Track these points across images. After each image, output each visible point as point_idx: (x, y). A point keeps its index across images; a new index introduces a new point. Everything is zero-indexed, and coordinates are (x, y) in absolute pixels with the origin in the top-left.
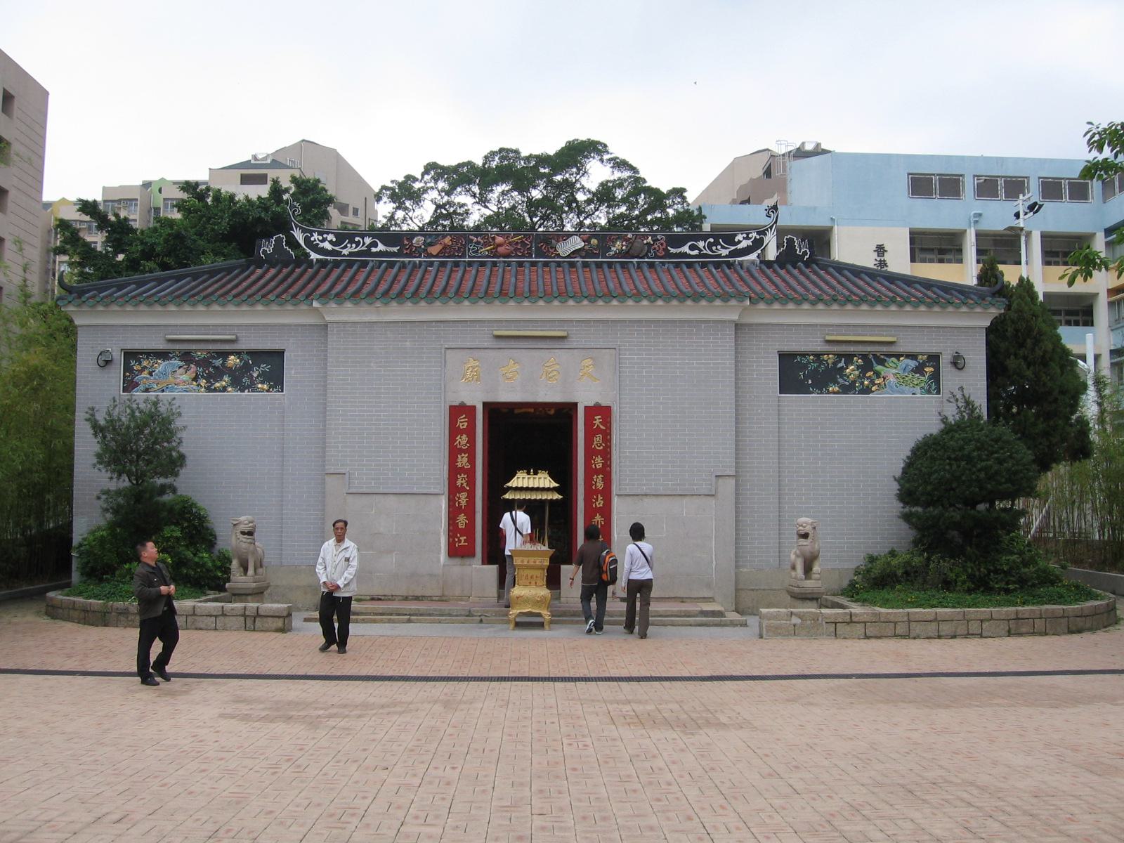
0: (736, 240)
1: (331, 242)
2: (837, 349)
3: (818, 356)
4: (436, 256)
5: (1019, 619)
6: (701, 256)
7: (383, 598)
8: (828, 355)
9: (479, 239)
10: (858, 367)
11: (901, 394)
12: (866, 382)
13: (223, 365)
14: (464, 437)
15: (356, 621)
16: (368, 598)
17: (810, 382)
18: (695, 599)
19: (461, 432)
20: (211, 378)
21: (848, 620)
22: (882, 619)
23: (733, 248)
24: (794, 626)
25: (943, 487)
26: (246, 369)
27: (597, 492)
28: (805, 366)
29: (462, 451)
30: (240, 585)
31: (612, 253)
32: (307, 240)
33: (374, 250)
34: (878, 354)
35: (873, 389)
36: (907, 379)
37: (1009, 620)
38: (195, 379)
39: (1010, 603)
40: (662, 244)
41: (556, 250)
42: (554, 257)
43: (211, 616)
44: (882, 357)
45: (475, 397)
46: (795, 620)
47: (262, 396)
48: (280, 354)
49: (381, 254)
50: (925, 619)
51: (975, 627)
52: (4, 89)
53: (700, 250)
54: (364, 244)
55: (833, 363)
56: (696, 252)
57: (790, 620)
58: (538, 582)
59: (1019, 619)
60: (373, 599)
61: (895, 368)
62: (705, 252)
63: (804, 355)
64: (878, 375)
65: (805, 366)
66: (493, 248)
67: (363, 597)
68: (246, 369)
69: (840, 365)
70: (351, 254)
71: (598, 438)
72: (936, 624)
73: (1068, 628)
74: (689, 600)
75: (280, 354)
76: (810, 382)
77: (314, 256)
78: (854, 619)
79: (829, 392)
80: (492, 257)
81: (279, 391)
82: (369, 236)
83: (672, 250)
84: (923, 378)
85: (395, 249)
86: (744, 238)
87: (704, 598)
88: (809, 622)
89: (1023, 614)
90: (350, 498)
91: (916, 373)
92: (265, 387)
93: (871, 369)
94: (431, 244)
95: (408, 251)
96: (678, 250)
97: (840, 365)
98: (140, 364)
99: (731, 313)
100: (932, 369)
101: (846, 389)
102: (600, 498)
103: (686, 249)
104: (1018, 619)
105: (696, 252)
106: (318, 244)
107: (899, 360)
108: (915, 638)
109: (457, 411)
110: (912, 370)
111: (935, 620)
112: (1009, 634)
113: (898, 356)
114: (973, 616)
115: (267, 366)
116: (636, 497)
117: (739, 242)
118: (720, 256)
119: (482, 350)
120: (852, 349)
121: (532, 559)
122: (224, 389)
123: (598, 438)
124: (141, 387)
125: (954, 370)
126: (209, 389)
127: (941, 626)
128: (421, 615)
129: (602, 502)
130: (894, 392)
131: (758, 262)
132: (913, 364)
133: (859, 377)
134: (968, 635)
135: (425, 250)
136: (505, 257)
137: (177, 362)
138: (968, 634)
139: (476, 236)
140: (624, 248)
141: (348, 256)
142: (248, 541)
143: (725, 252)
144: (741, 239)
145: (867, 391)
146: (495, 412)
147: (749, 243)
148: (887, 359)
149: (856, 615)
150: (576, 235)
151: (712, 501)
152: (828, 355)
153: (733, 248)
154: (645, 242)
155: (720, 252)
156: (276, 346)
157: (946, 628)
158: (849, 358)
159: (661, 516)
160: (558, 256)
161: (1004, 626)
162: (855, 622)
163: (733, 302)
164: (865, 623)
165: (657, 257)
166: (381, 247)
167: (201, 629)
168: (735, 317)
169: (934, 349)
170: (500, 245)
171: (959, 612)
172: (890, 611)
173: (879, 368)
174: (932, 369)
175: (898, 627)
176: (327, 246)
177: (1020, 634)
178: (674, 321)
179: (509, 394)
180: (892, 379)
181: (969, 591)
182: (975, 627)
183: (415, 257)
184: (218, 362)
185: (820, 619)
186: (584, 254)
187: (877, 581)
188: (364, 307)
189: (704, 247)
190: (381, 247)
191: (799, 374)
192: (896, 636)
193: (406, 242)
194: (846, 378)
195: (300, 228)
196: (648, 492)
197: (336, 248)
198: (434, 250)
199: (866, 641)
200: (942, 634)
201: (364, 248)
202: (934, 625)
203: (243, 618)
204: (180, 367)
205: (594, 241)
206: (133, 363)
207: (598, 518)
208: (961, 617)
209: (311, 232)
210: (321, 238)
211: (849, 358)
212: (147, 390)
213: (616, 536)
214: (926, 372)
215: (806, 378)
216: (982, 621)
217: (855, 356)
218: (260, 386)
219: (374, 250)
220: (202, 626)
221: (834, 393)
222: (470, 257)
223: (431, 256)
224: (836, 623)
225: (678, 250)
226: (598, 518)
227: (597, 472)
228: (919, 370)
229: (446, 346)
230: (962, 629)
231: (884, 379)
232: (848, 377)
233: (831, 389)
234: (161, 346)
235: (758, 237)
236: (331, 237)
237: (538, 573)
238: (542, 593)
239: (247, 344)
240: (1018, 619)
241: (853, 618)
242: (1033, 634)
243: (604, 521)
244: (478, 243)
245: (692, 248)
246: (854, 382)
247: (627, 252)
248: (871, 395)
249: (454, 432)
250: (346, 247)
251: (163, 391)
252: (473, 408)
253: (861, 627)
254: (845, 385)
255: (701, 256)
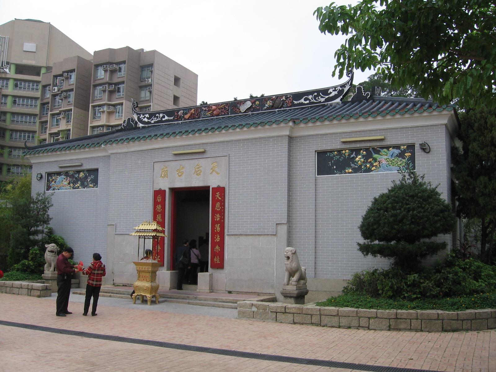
0: (329, 92)
1: (147, 118)
2: (348, 146)
3: (339, 151)
4: (188, 119)
5: (398, 319)
6: (311, 103)
7: (127, 285)
8: (345, 150)
9: (206, 109)
10: (363, 156)
11: (390, 171)
12: (368, 165)
13: (78, 176)
14: (160, 206)
15: (103, 296)
16: (122, 285)
17: (335, 167)
18: (265, 293)
19: (158, 203)
20: (75, 183)
21: (284, 311)
22: (304, 312)
23: (327, 97)
24: (253, 312)
25: (371, 228)
26: (86, 177)
27: (217, 233)
28: (332, 158)
29: (158, 213)
30: (46, 275)
31: (265, 108)
32: (139, 118)
33: (163, 119)
34: (375, 147)
35: (373, 169)
36: (393, 161)
37: (390, 319)
38: (69, 184)
39: (390, 307)
40: (290, 100)
41: (239, 110)
42: (239, 113)
43: (18, 288)
44: (378, 149)
45: (165, 185)
46: (254, 309)
47: (89, 191)
48: (97, 170)
49: (166, 121)
50: (331, 314)
51: (363, 322)
52: (175, 76)
53: (310, 100)
54: (160, 117)
55: (349, 155)
56: (308, 102)
57: (251, 309)
58: (147, 279)
59: (398, 319)
60: (123, 286)
61: (386, 155)
62: (312, 101)
63: (331, 151)
64: (375, 160)
65: (332, 158)
66: (212, 112)
67: (120, 284)
68: (86, 177)
69: (352, 156)
70: (155, 122)
71: (218, 204)
72: (338, 317)
73: (443, 328)
74: (262, 294)
75: (97, 170)
76: (335, 167)
77: (141, 125)
78: (287, 311)
79: (346, 173)
80: (212, 117)
81: (97, 187)
82: (162, 113)
83: (295, 102)
84: (404, 160)
85: (172, 118)
86: (333, 91)
87: (270, 293)
88: (261, 311)
89: (401, 315)
90: (116, 236)
91: (399, 157)
92: (92, 186)
93: (371, 156)
94: (186, 114)
95: (177, 118)
96: (299, 102)
97: (352, 156)
98: (52, 178)
99: (284, 130)
100: (410, 154)
101: (357, 170)
102: (218, 236)
103: (302, 101)
104: (397, 318)
105: (308, 102)
106: (142, 120)
107: (388, 150)
108: (324, 326)
109: (159, 194)
110: (397, 156)
111: (338, 315)
112: (390, 329)
113: (388, 148)
114: (363, 315)
115: (90, 177)
116: (236, 236)
117: (331, 93)
118: (320, 102)
119: (169, 162)
120: (358, 145)
121: (144, 267)
122: (78, 188)
123: (218, 204)
124: (52, 189)
125: (423, 153)
126: (74, 188)
127: (340, 320)
128: (121, 294)
129: (219, 239)
130: (385, 170)
131: (341, 103)
132: (397, 152)
133: (364, 162)
134: (359, 327)
135: (183, 117)
136: (217, 116)
137: (63, 177)
138: (359, 326)
139: (205, 107)
140: (271, 104)
141: (154, 123)
142: (52, 255)
143: (323, 100)
144: (332, 91)
145: (369, 170)
146: (175, 192)
147: (336, 93)
148: (381, 150)
149: (288, 308)
150: (249, 101)
151: (275, 238)
152: (345, 150)
153: (327, 97)
154: (282, 99)
155: (320, 100)
156: (96, 167)
157: (344, 321)
158: (357, 151)
159: (250, 247)
160: (240, 112)
161: (386, 323)
162: (287, 313)
163: (282, 125)
164: (294, 313)
165: (287, 107)
166: (166, 118)
167: (14, 294)
168: (287, 133)
169: (410, 141)
170: (214, 110)
171: (353, 311)
172: (365, 310)
173: (375, 156)
174: (410, 154)
175: (314, 318)
176: (146, 120)
177: (399, 330)
178: (255, 139)
179: (180, 184)
180: (384, 162)
181: (390, 297)
182: (363, 322)
183: (180, 121)
184: (77, 176)
185: (268, 309)
186: (252, 110)
187: (365, 291)
188: (120, 145)
189: (312, 98)
190: (166, 118)
191: (328, 163)
192: (312, 324)
193: (176, 114)
194: (356, 163)
195: (136, 113)
196: (242, 233)
197: (149, 121)
198: (187, 116)
199: (294, 325)
200: (341, 325)
201: (160, 119)
202: (336, 319)
203: (27, 290)
204: (64, 179)
205: (257, 103)
206: (50, 178)
207: (217, 247)
208: (355, 314)
209: (140, 114)
210: (143, 116)
211: (357, 151)
212: (54, 190)
213: (226, 257)
214: (406, 156)
215: (333, 166)
216: (369, 318)
217: (361, 149)
218: (90, 185)
219: (163, 119)
220: (15, 292)
221: (349, 173)
222: (202, 118)
223: (185, 119)
224: (276, 313)
225: (299, 102)
226: (217, 247)
227: (217, 222)
228: (401, 155)
229: (154, 161)
230: (355, 323)
231: (379, 162)
232: (357, 163)
233: (347, 171)
234: (57, 169)
235: (341, 89)
236: (147, 116)
237: (148, 275)
238: (147, 285)
239: (87, 166)
240: (397, 318)
241: (286, 310)
242: (410, 330)
243: (220, 249)
244: (205, 110)
245: (305, 100)
246: (361, 165)
247: (273, 106)
248: (371, 173)
249: (156, 203)
250: (153, 119)
251: (59, 190)
252: (165, 191)
253: (290, 316)
254: (355, 168)
255: (311, 103)
